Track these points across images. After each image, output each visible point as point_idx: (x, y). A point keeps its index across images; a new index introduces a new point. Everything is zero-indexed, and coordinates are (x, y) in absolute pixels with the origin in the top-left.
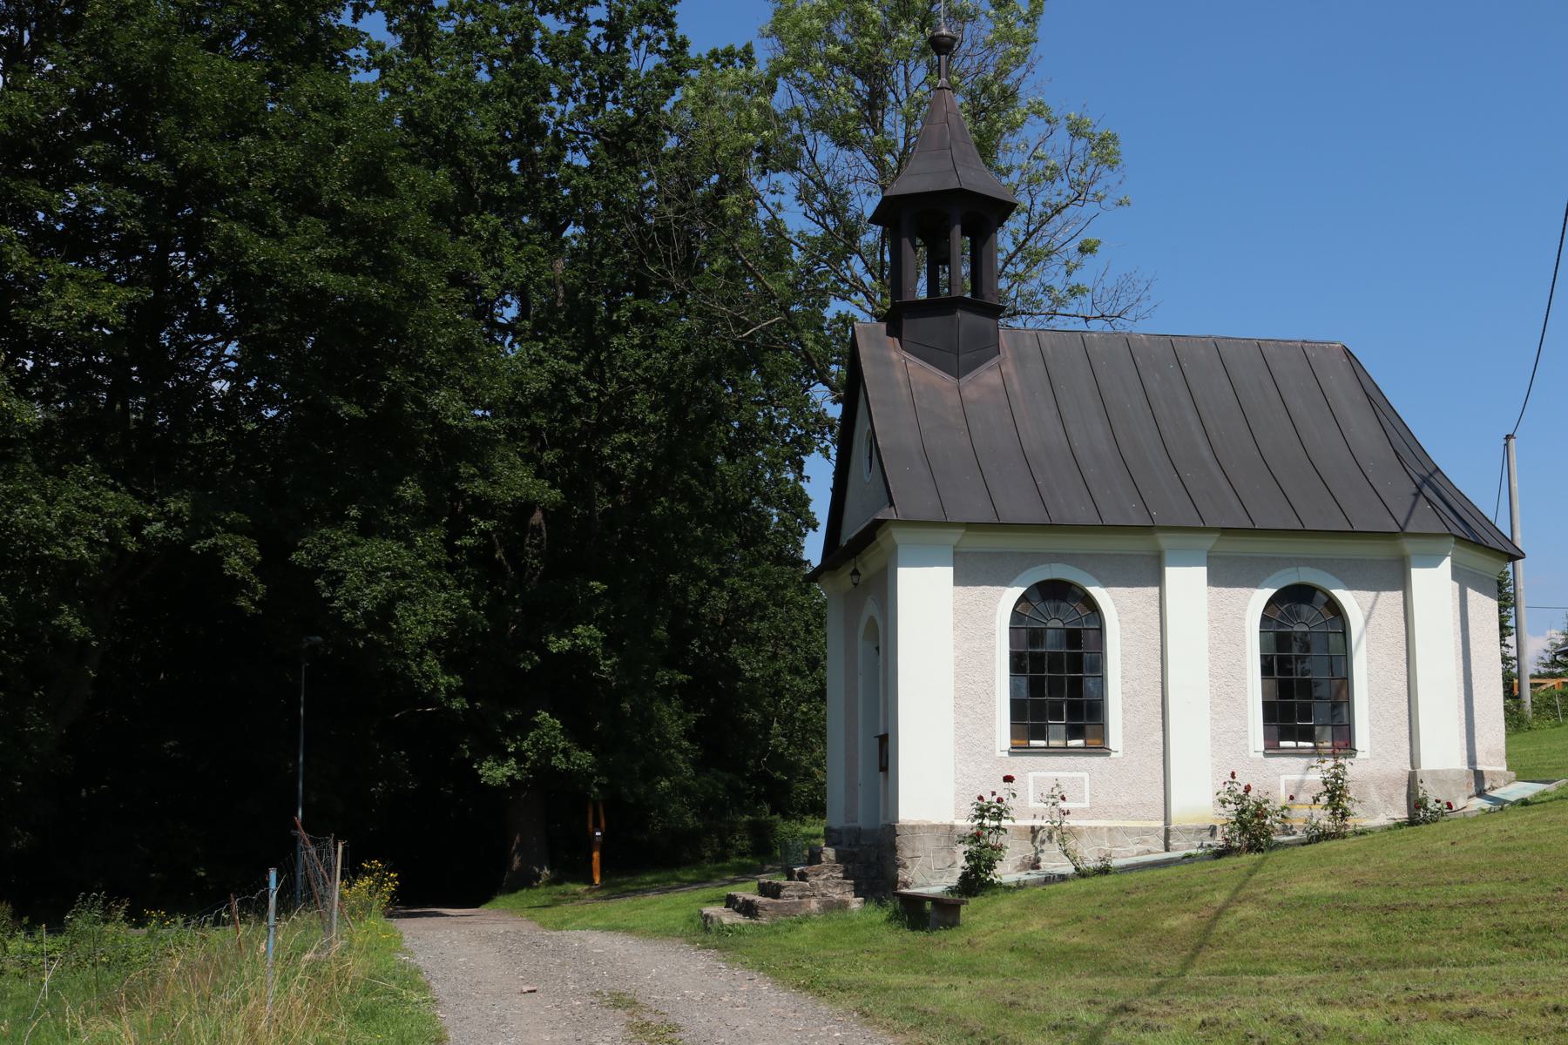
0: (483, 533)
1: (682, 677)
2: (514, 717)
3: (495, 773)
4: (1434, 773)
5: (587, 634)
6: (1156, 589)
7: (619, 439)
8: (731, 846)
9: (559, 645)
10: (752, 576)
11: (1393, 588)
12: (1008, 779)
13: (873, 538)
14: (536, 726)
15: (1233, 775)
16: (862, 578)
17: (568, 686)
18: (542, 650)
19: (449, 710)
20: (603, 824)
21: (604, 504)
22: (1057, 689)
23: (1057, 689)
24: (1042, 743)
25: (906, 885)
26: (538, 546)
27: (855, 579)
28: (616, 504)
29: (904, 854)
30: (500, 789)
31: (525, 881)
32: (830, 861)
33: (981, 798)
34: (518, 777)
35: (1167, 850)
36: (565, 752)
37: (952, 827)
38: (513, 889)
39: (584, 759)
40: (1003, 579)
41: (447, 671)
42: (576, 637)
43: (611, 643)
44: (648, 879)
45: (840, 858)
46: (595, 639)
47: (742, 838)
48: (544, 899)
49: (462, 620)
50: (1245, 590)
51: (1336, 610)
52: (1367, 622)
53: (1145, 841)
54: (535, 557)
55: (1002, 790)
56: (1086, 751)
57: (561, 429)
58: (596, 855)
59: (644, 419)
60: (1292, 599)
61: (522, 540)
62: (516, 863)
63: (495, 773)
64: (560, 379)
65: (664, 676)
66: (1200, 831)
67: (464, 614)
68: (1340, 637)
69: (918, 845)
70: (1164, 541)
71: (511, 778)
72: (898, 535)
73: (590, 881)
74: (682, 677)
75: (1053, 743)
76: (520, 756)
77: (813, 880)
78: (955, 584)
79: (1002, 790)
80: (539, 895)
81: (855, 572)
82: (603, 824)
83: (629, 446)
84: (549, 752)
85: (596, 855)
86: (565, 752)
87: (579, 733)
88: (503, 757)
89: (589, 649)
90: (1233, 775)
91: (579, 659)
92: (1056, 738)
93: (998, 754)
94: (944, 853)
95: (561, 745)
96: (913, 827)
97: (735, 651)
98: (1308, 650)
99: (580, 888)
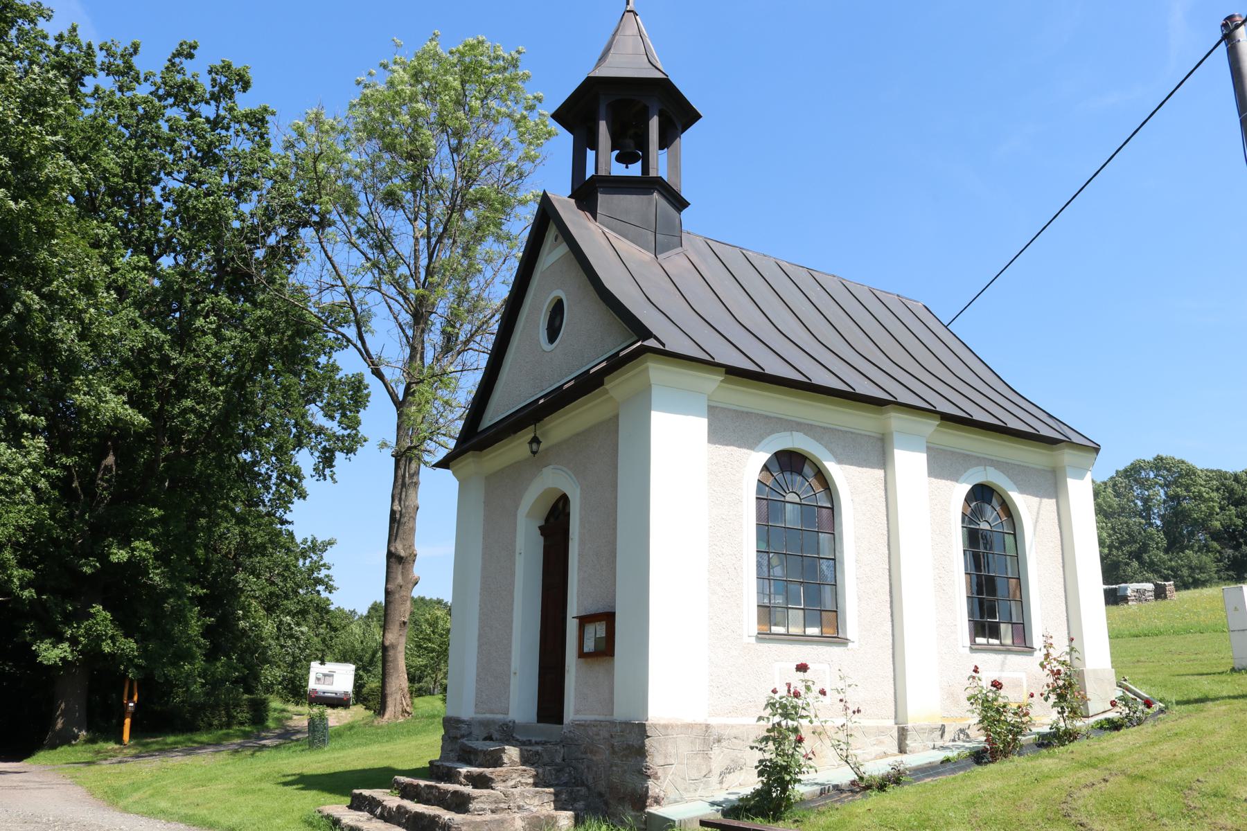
0: (64, 467)
1: (202, 592)
2: (75, 609)
3: (51, 653)
4: (1094, 671)
5: (143, 547)
6: (880, 473)
7: (188, 403)
8: (234, 717)
9: (119, 555)
10: (260, 525)
11: (1049, 497)
12: (802, 668)
13: (602, 384)
14: (93, 616)
15: (976, 670)
16: (542, 446)
17: (121, 592)
18: (104, 558)
19: (18, 599)
20: (136, 698)
21: (167, 450)
22: (799, 570)
23: (799, 570)
24: (781, 630)
25: (657, 801)
26: (107, 481)
27: (535, 446)
28: (178, 452)
29: (655, 760)
30: (54, 667)
31: (67, 739)
32: (513, 763)
33: (774, 691)
34: (70, 658)
35: (902, 750)
36: (112, 638)
37: (707, 726)
38: (53, 747)
39: (130, 645)
40: (751, 443)
41: (22, 564)
42: (133, 550)
43: (162, 558)
44: (171, 739)
45: (525, 760)
46: (149, 552)
47: (242, 711)
48: (88, 756)
49: (39, 527)
50: (948, 483)
51: (1008, 511)
52: (1035, 527)
53: (881, 742)
54: (105, 489)
55: (797, 680)
56: (822, 639)
57: (145, 374)
58: (128, 721)
59: (206, 391)
60: (982, 495)
61: (96, 474)
62: (60, 724)
63: (51, 653)
64: (149, 343)
65: (191, 589)
66: (932, 730)
67: (43, 521)
68: (1012, 537)
69: (671, 749)
70: (896, 421)
71: (63, 659)
72: (656, 371)
73: (119, 741)
74: (202, 592)
75: (793, 630)
76: (74, 641)
77: (499, 786)
78: (709, 441)
79: (797, 680)
80: (79, 751)
81: (535, 440)
82: (136, 698)
83: (193, 410)
84: (100, 638)
85: (128, 721)
86: (112, 638)
87: (126, 624)
88: (59, 638)
89: (144, 560)
90: (976, 670)
91: (135, 568)
92: (796, 625)
93: (746, 640)
94: (699, 760)
95: (110, 633)
96: (666, 727)
97: (240, 576)
98: (991, 549)
99: (111, 746)
